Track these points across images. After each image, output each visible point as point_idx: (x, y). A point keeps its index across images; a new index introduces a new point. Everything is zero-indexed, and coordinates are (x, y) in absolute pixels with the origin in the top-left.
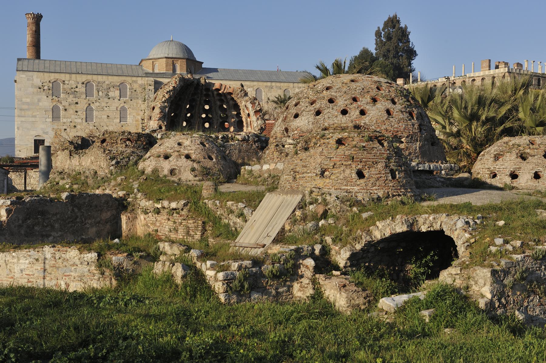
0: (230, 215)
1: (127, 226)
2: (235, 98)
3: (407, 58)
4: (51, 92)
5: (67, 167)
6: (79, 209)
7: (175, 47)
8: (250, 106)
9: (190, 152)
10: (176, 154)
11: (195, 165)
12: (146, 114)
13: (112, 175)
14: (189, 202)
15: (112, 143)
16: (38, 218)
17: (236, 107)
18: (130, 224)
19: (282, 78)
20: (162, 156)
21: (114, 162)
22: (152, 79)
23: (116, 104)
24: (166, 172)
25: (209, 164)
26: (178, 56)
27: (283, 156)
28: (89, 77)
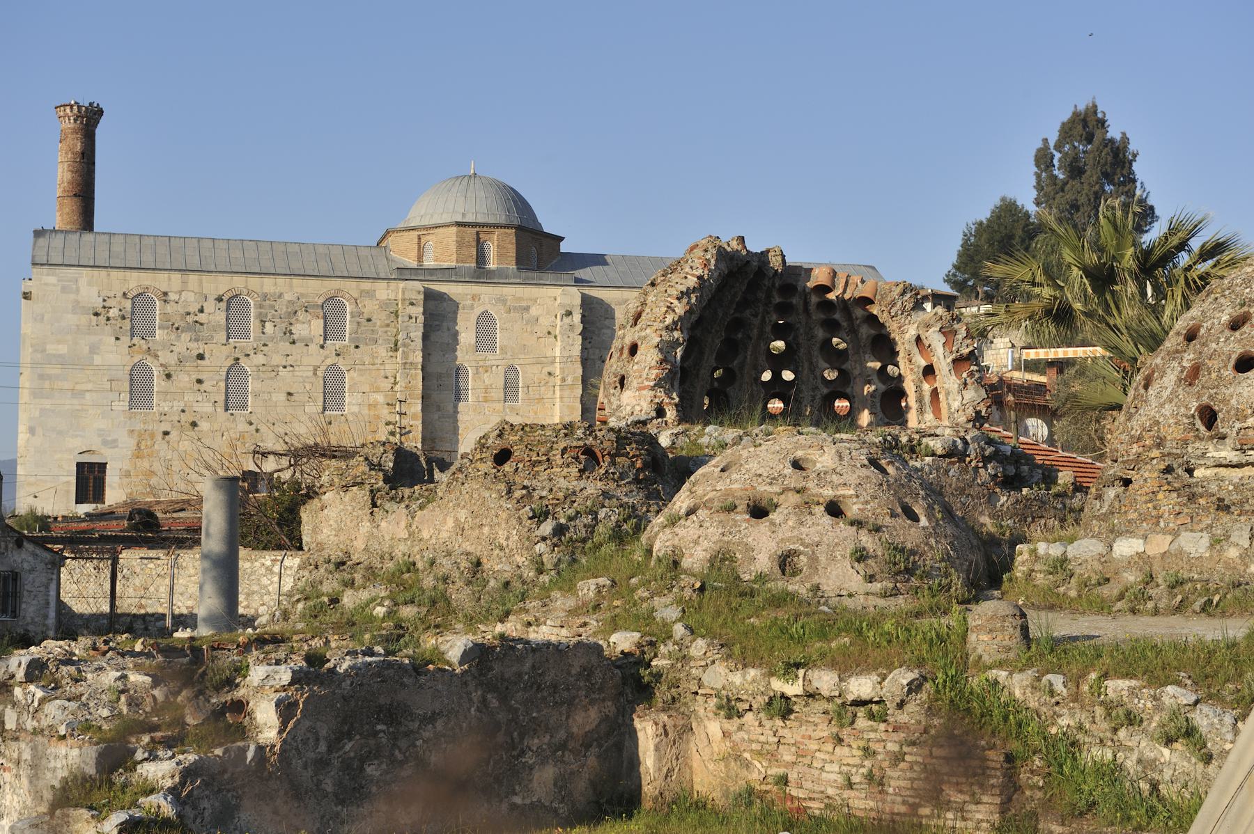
0: (1122, 733)
1: (659, 759)
2: (883, 318)
5: (360, 544)
6: (504, 699)
7: (482, 194)
8: (935, 339)
9: (841, 492)
10: (793, 498)
11: (867, 540)
12: (397, 388)
13: (540, 571)
14: (925, 679)
15: (534, 464)
16: (375, 734)
17: (884, 346)
18: (671, 753)
20: (742, 507)
21: (547, 528)
22: (419, 286)
23: (313, 357)
24: (764, 562)
25: (911, 535)
26: (491, 220)
27: (1206, 509)
28: (238, 282)
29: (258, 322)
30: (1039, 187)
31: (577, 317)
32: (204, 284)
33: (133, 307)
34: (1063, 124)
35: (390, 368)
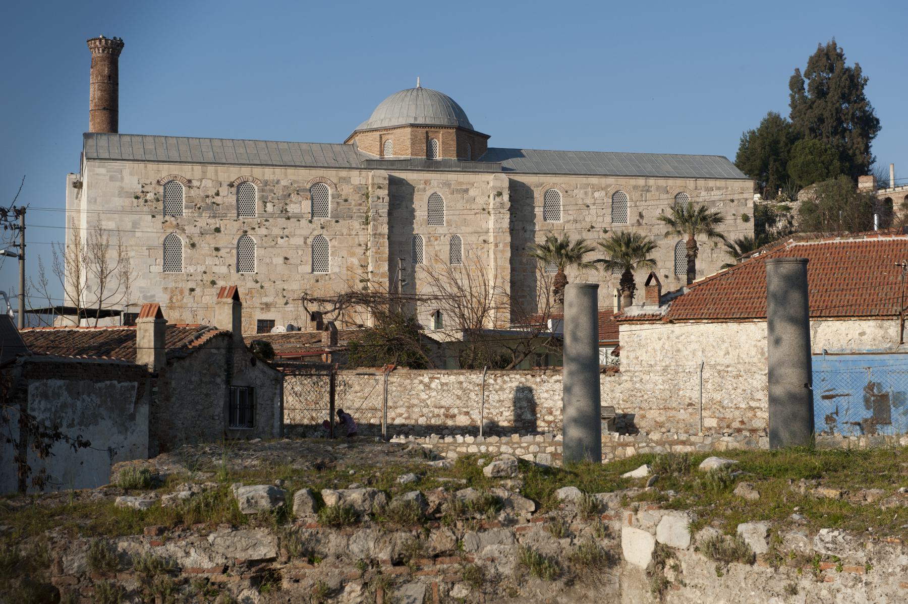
3: (860, 134)
4: (160, 205)
7: (429, 102)
19: (667, 168)
22: (385, 173)
23: (304, 230)
26: (437, 122)
28: (245, 171)
29: (261, 202)
30: (793, 105)
31: (506, 197)
32: (220, 174)
33: (165, 192)
34: (811, 58)
35: (362, 239)
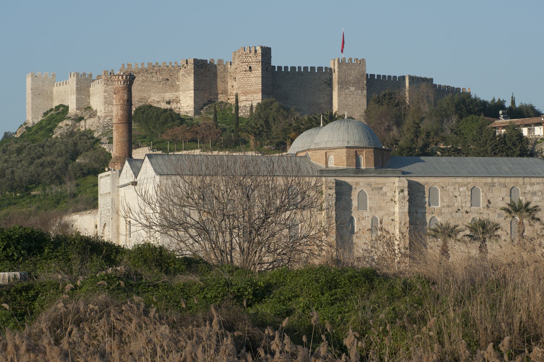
7: (356, 131)
22: (332, 179)
31: (406, 193)
